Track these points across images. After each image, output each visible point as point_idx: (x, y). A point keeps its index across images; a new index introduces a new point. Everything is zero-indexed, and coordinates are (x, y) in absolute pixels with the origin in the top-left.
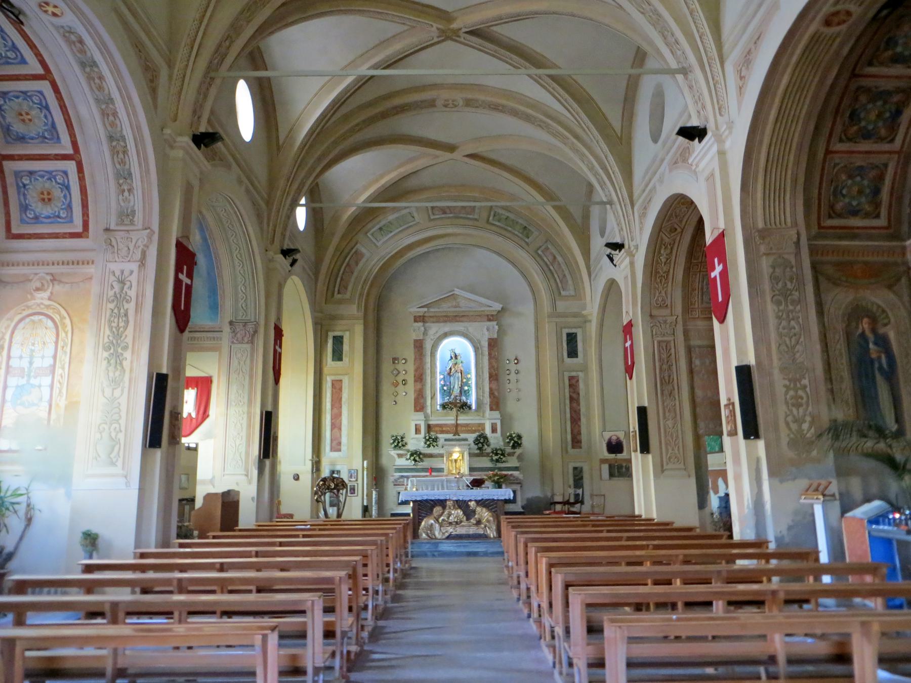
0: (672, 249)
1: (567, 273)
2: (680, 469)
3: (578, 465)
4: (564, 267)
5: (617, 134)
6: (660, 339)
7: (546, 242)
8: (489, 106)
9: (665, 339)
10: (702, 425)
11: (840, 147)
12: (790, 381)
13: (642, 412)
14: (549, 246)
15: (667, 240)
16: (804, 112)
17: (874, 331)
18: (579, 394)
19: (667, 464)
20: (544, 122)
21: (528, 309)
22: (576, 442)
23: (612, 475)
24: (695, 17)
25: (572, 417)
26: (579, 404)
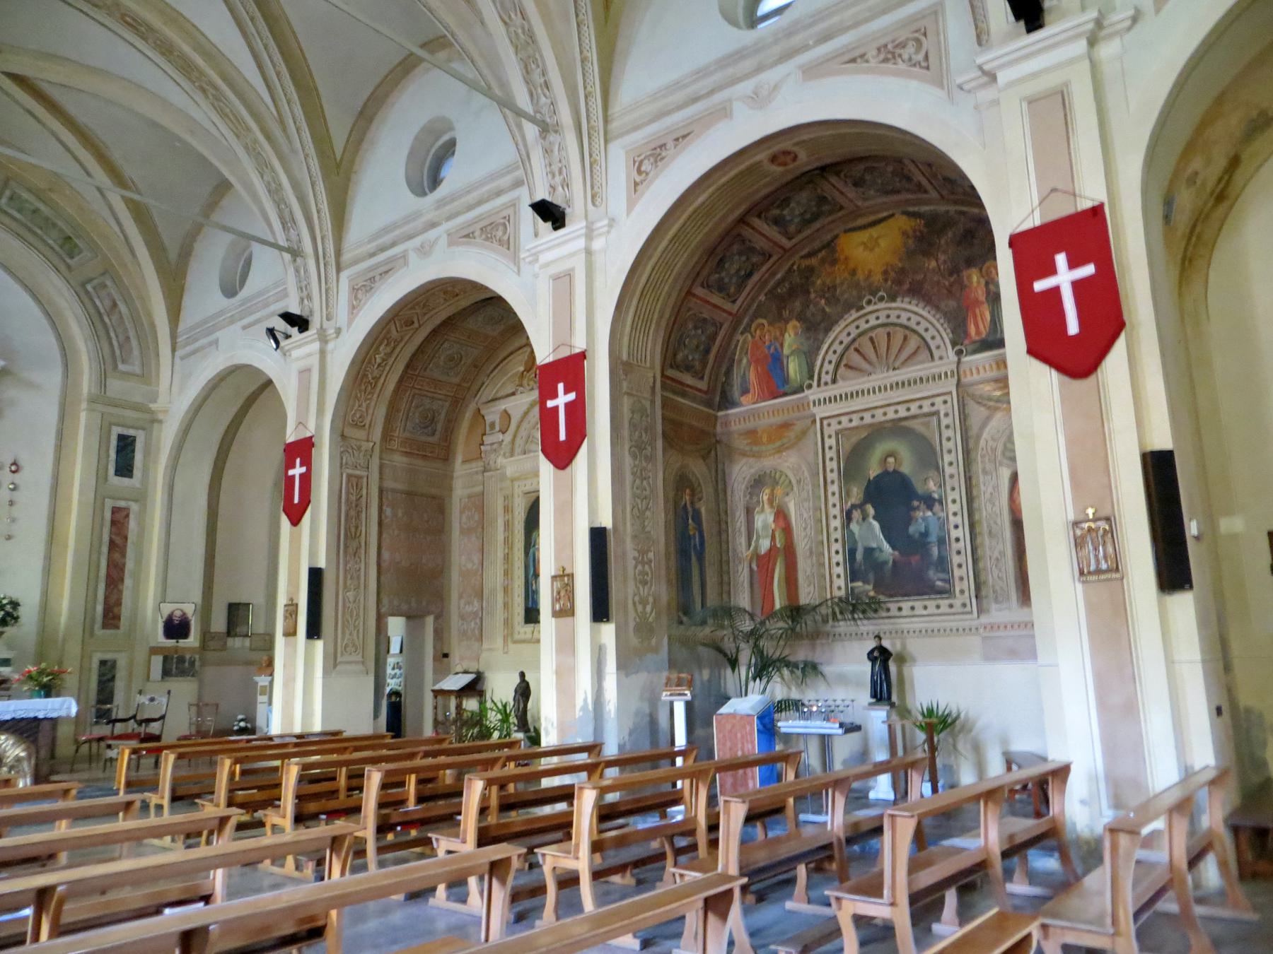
0: (394, 348)
1: (132, 334)
2: (356, 663)
3: (108, 656)
4: (129, 325)
5: (335, 159)
6: (350, 471)
7: (103, 274)
8: (123, 16)
9: (357, 472)
10: (385, 601)
11: (699, 291)
12: (639, 552)
13: (316, 575)
14: (109, 283)
15: (394, 334)
16: (698, 239)
17: (692, 503)
18: (126, 538)
19: (342, 655)
20: (216, 88)
21: (53, 379)
22: (111, 617)
23: (166, 673)
24: (587, 68)
25: (108, 576)
26: (123, 555)
